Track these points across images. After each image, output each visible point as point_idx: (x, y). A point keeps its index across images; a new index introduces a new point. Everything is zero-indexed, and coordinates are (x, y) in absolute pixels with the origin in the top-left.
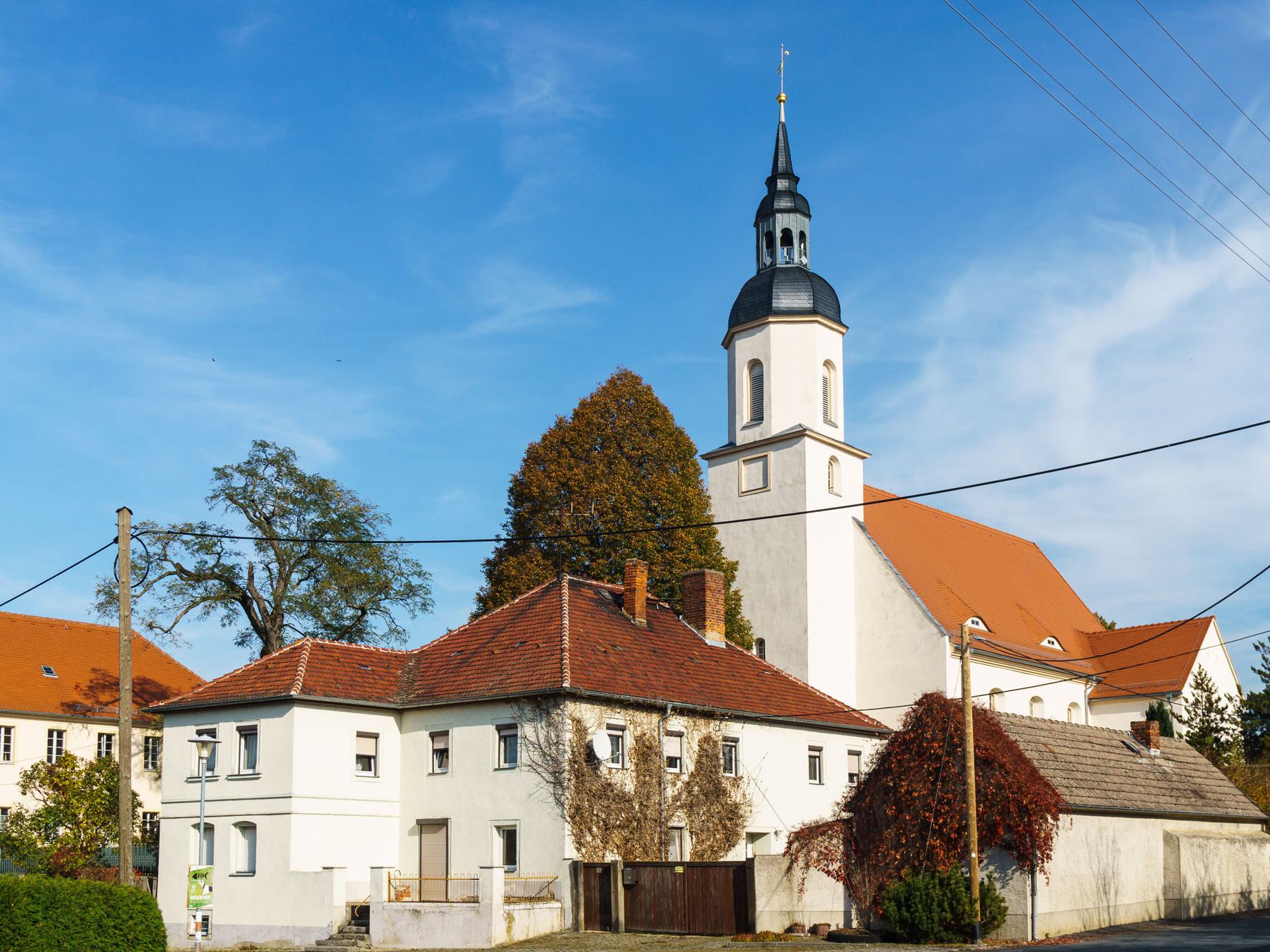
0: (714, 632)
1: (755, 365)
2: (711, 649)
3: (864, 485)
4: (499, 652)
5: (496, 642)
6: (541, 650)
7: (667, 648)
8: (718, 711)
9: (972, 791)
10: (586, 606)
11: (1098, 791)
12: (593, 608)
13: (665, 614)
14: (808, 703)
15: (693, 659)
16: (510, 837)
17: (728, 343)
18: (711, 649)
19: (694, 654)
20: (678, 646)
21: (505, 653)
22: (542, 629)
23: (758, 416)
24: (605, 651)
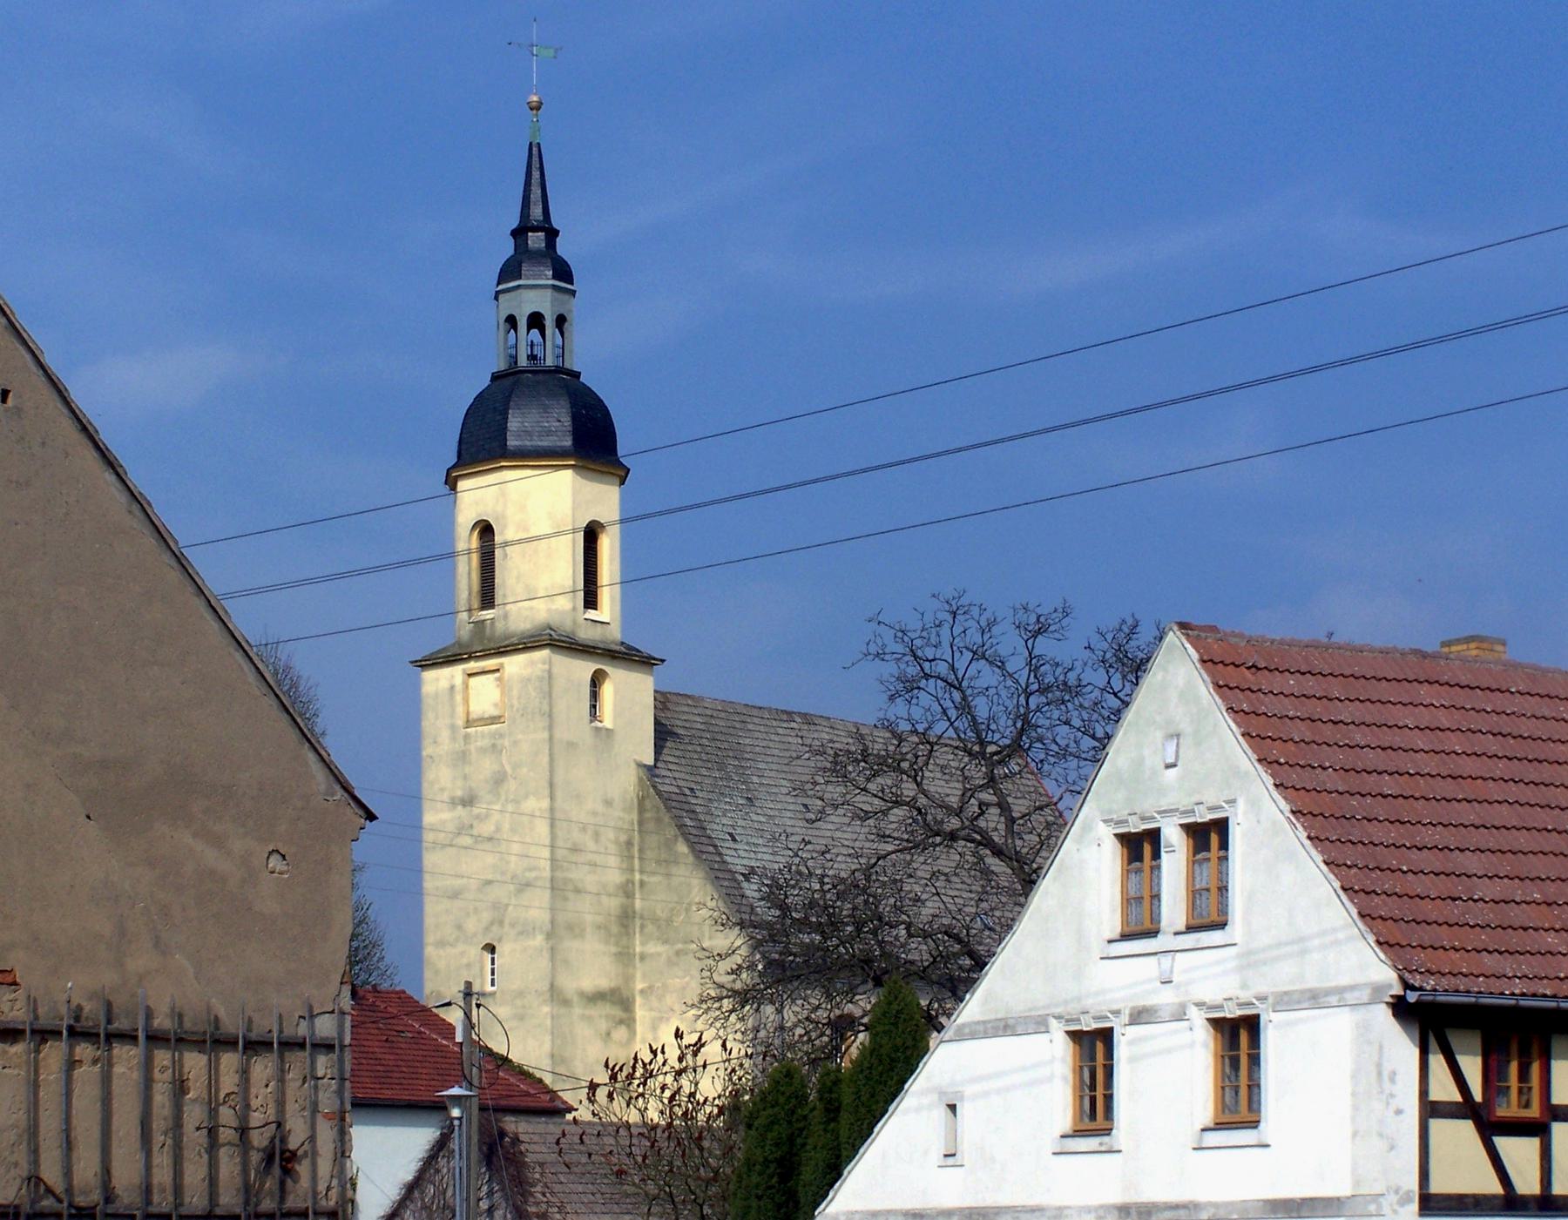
23: (487, 597)
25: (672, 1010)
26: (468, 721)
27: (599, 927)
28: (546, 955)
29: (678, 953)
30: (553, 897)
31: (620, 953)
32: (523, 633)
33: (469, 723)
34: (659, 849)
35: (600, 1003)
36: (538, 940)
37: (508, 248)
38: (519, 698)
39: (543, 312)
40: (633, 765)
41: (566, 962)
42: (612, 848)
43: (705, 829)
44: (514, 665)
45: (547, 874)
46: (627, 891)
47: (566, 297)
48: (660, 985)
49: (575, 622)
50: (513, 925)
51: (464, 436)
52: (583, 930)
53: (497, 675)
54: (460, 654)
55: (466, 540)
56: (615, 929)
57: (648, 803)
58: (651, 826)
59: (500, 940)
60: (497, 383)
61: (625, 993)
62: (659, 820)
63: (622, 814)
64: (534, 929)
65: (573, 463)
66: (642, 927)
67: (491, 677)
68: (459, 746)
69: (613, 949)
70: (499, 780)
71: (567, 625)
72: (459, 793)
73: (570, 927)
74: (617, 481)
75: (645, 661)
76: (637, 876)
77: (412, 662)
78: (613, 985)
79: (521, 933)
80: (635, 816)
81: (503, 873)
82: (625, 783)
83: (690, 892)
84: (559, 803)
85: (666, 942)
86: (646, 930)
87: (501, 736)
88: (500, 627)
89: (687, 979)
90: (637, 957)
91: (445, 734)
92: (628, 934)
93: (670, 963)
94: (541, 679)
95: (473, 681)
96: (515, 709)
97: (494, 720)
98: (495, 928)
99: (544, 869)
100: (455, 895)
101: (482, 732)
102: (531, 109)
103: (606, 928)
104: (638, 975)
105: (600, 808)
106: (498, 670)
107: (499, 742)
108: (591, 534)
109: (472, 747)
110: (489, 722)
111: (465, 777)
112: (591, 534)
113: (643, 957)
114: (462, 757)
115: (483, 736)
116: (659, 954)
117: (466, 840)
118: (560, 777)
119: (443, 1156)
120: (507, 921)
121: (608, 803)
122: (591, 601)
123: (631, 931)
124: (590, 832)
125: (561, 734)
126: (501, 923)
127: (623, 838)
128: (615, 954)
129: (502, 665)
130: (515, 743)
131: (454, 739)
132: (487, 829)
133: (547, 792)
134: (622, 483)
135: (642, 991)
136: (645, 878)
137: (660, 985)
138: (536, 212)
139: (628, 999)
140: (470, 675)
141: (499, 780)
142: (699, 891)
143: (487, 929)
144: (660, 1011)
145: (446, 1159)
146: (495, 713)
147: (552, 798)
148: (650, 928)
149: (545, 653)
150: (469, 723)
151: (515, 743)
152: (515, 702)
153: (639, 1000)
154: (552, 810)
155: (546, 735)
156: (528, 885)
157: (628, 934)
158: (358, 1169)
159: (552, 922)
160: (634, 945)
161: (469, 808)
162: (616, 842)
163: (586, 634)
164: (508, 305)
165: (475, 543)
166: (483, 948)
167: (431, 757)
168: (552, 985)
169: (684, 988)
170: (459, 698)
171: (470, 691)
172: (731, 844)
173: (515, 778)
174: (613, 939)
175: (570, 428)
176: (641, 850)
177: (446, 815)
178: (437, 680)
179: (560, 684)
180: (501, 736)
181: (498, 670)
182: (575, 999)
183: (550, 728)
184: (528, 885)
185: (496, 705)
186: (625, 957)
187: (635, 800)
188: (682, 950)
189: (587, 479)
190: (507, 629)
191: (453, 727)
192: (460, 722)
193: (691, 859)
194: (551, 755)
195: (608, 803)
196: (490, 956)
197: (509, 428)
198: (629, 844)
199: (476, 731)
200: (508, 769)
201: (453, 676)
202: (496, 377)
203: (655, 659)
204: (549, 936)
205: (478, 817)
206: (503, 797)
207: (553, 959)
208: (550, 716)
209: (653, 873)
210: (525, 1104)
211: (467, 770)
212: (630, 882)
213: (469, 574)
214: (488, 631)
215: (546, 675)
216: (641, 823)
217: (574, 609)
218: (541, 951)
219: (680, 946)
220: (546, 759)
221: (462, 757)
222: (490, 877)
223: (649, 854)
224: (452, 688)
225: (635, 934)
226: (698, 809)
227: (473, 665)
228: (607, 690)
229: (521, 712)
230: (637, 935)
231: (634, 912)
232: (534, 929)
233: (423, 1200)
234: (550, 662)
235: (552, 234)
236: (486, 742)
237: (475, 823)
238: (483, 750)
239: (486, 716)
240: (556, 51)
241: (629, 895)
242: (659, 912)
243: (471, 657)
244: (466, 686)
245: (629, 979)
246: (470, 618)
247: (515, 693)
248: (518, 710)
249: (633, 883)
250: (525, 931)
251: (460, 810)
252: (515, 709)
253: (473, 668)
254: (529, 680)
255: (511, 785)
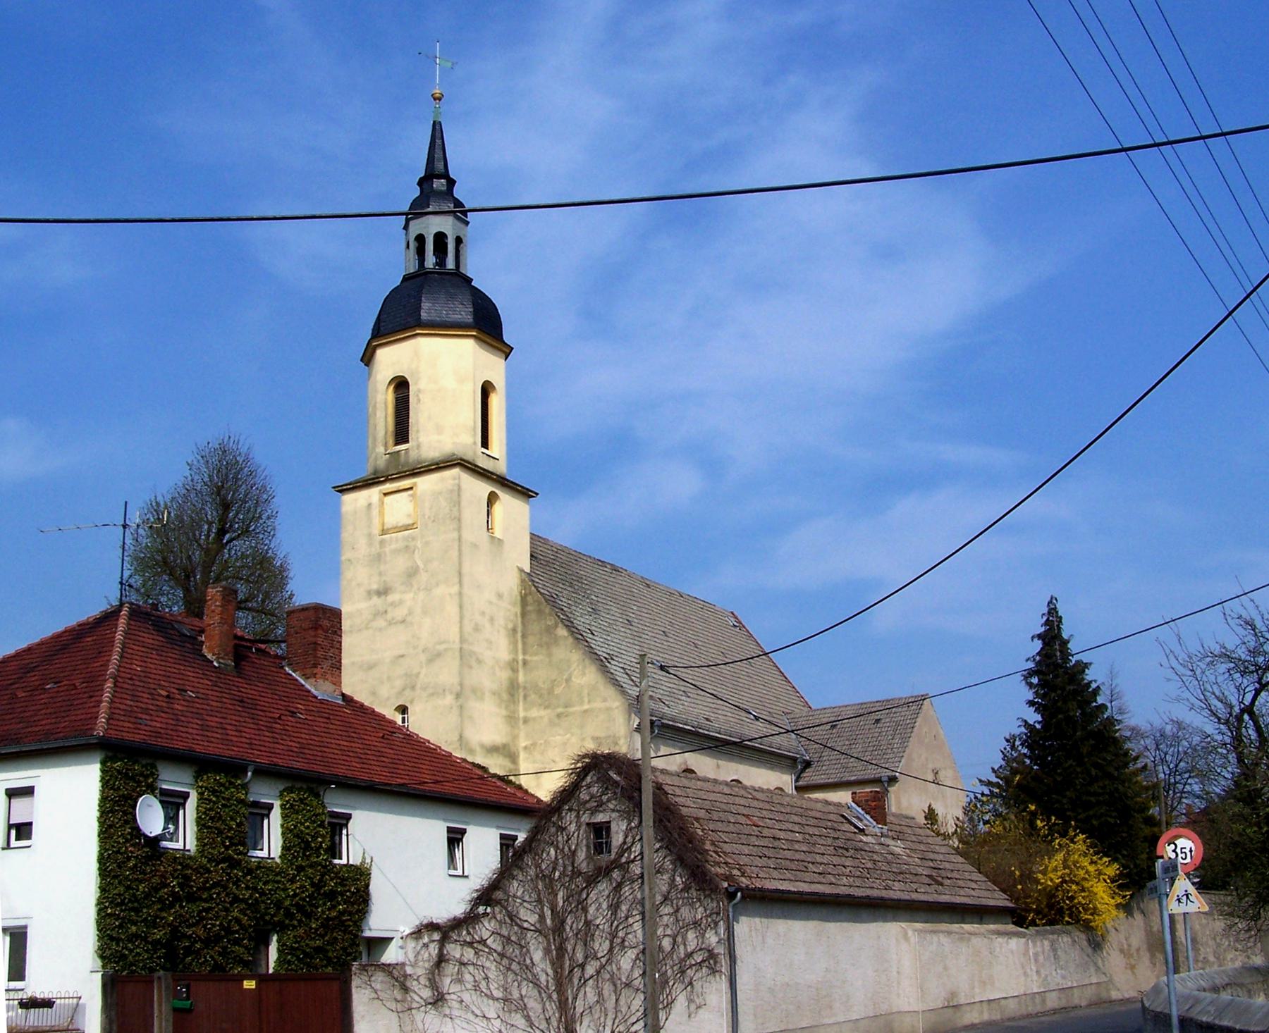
0: (326, 682)
1: (401, 385)
2: (322, 703)
3: (534, 537)
4: (23, 695)
5: (24, 682)
6: (78, 691)
7: (259, 698)
8: (941, 1011)
9: (299, 679)
10: (151, 641)
11: (843, 888)
12: (161, 644)
13: (263, 658)
14: (447, 773)
15: (295, 713)
16: (18, 938)
17: (368, 358)
18: (322, 703)
19: (297, 708)
20: (276, 697)
21: (31, 695)
22: (84, 666)
23: (402, 432)
24: (168, 697)
25: (554, 761)
26: (383, 530)
27: (494, 694)
28: (455, 711)
29: (559, 716)
30: (462, 665)
31: (509, 716)
32: (433, 459)
33: (384, 532)
34: (541, 634)
35: (495, 755)
36: (449, 699)
37: (416, 192)
38: (431, 509)
39: (442, 230)
40: (516, 570)
41: (471, 718)
42: (503, 632)
43: (572, 623)
44: (425, 483)
45: (457, 646)
46: (513, 666)
47: (463, 226)
48: (542, 742)
49: (475, 453)
50: (424, 689)
51: (381, 317)
52: (483, 694)
53: (410, 492)
54: (378, 478)
55: (384, 399)
56: (505, 696)
57: (529, 599)
58: (533, 616)
59: (411, 702)
60: (405, 284)
61: (513, 749)
62: (540, 612)
63: (509, 607)
64: (444, 690)
65: (474, 333)
66: (525, 697)
67: (405, 494)
68: (376, 549)
69: (504, 712)
70: (412, 573)
71: (469, 457)
72: (375, 587)
73: (474, 691)
74: (504, 356)
75: (525, 493)
76: (521, 657)
77: (334, 488)
78: (504, 741)
79: (432, 694)
80: (518, 610)
81: (415, 648)
82: (511, 584)
83: (569, 667)
84: (466, 590)
85: (546, 707)
86: (529, 699)
87: (413, 539)
88: (413, 455)
89: (568, 736)
90: (521, 722)
91: (363, 542)
92: (514, 702)
93: (552, 724)
94: (452, 491)
95: (388, 499)
96: (426, 517)
97: (406, 528)
98: (408, 692)
99: (454, 642)
100: (371, 667)
101: (397, 538)
102: (435, 99)
103: (499, 695)
104: (522, 735)
105: (494, 600)
106: (411, 488)
107: (412, 544)
108: (486, 390)
109: (387, 550)
110: (403, 529)
111: (380, 574)
112: (486, 390)
113: (526, 721)
114: (379, 558)
115: (397, 540)
116: (541, 717)
117: (381, 623)
118: (466, 570)
119: (570, 810)
120: (419, 686)
121: (500, 596)
122: (485, 443)
123: (516, 700)
124: (487, 617)
125: (467, 535)
126: (413, 688)
127: (510, 626)
128: (505, 717)
129: (415, 484)
130: (427, 543)
131: (370, 544)
132: (399, 613)
133: (456, 580)
134: (506, 360)
135: (526, 748)
136: (528, 657)
137: (542, 742)
138: (439, 166)
139: (514, 754)
140: (385, 494)
141: (412, 573)
142: (578, 666)
143: (401, 693)
144: (543, 763)
145: (574, 814)
146: (411, 522)
147: (460, 582)
148: (533, 697)
149: (456, 471)
150: (384, 532)
151: (427, 543)
152: (427, 513)
153: (522, 755)
154: (460, 594)
155: (455, 535)
156: (439, 655)
157: (514, 702)
158: (372, 858)
159: (461, 685)
160: (518, 711)
161: (383, 597)
162: (506, 628)
163: (483, 463)
164: (417, 227)
165: (390, 396)
166: (396, 709)
167: (349, 560)
168: (461, 737)
169: (565, 744)
170: (375, 512)
171: (385, 506)
172: (591, 636)
173: (426, 571)
174: (503, 706)
175: (471, 310)
176: (524, 636)
177: (363, 605)
178: (354, 502)
179: (466, 496)
180: (413, 539)
181: (411, 488)
182: (478, 749)
183: (459, 529)
184: (439, 655)
185: (409, 516)
186: (511, 719)
187: (519, 598)
188: (562, 713)
189: (481, 347)
190: (420, 456)
191: (370, 536)
192: (376, 530)
193: (571, 640)
194: (460, 550)
195: (500, 596)
196: (401, 716)
197: (423, 307)
198: (514, 630)
199: (391, 537)
200: (420, 563)
201: (370, 497)
202: (406, 279)
203: (532, 491)
204: (458, 696)
205: (393, 604)
206: (416, 587)
207: (461, 715)
208: (459, 520)
209: (536, 654)
210: (515, 803)
211: (382, 568)
212: (515, 660)
213: (386, 417)
214: (402, 459)
215: (456, 488)
216: (524, 614)
217: (475, 443)
218: (452, 708)
219: (560, 710)
220: (456, 554)
221: (379, 558)
222: (401, 652)
223: (531, 639)
224: (370, 505)
225: (519, 702)
226: (565, 609)
227: (389, 487)
228: (497, 508)
229: (432, 519)
230: (521, 704)
231: (518, 684)
232: (444, 690)
233: (538, 866)
234: (459, 478)
235: (451, 183)
236: (401, 544)
237: (389, 609)
238: (397, 552)
239: (400, 524)
240: (453, 64)
241: (515, 671)
242: (541, 684)
243: (388, 479)
244: (382, 503)
245: (515, 737)
246: (386, 450)
247: (427, 505)
248: (429, 517)
249: (517, 662)
250: (437, 692)
251: (375, 599)
252: (426, 517)
253: (388, 489)
254: (440, 493)
255: (423, 577)
